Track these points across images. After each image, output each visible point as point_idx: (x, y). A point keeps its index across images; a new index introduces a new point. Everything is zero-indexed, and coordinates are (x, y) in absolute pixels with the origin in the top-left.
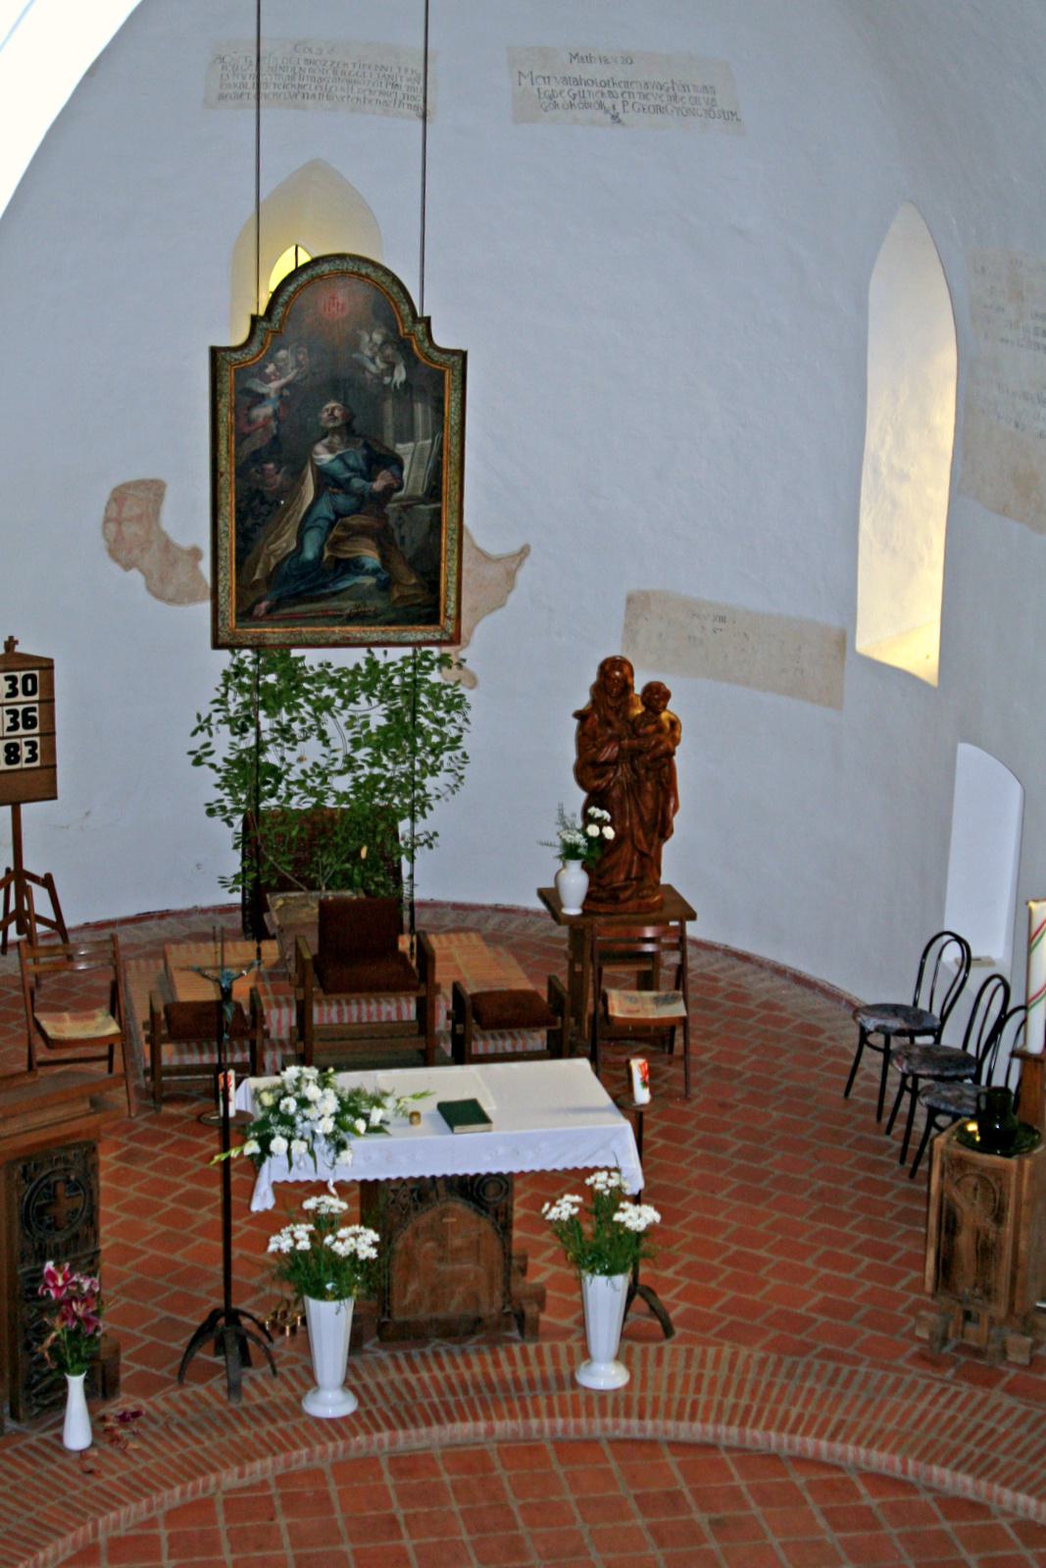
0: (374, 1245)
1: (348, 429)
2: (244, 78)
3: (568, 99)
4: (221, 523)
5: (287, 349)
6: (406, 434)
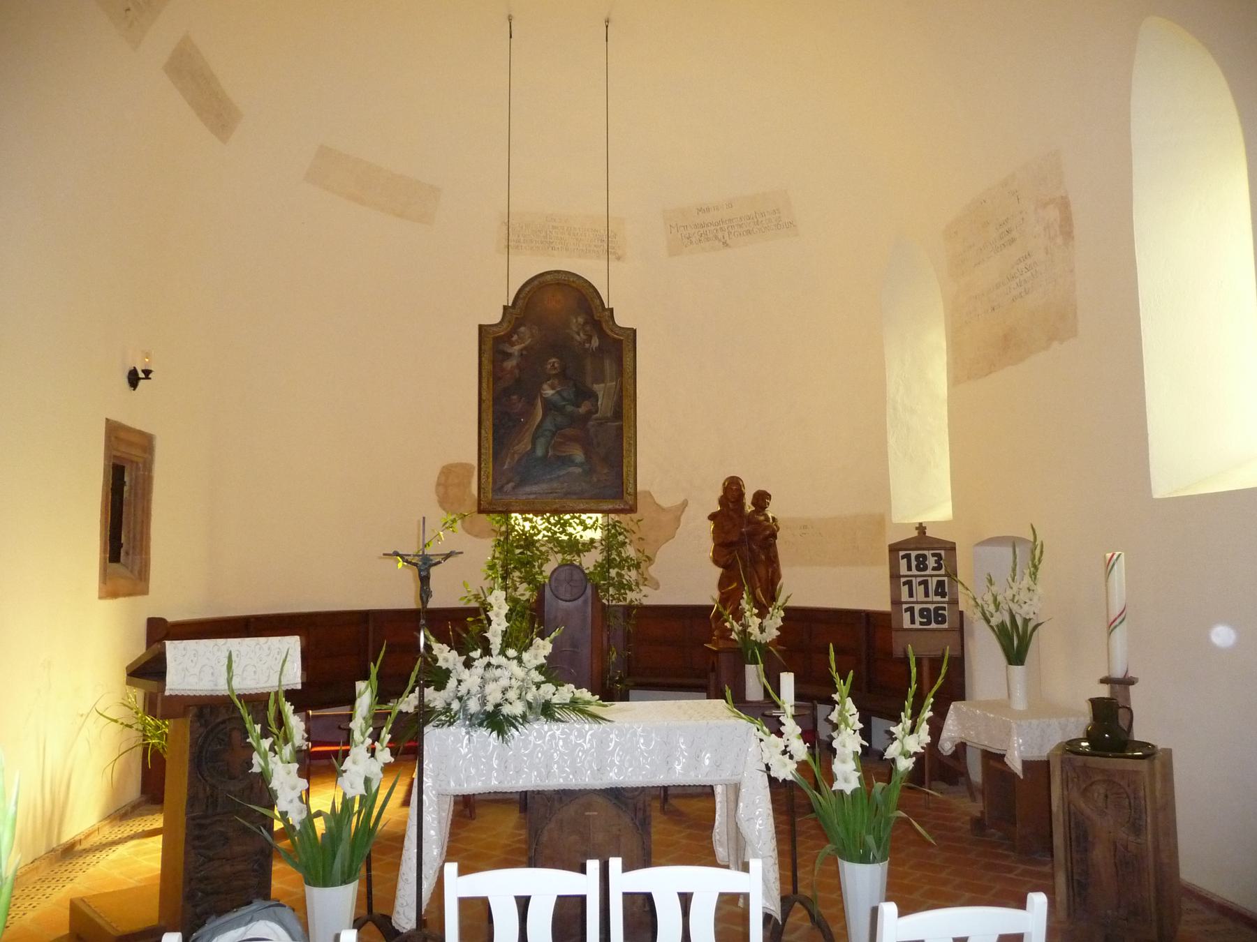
0: (291, 705)
1: (563, 375)
2: (519, 236)
3: (698, 237)
4: (483, 432)
5: (525, 326)
6: (600, 379)
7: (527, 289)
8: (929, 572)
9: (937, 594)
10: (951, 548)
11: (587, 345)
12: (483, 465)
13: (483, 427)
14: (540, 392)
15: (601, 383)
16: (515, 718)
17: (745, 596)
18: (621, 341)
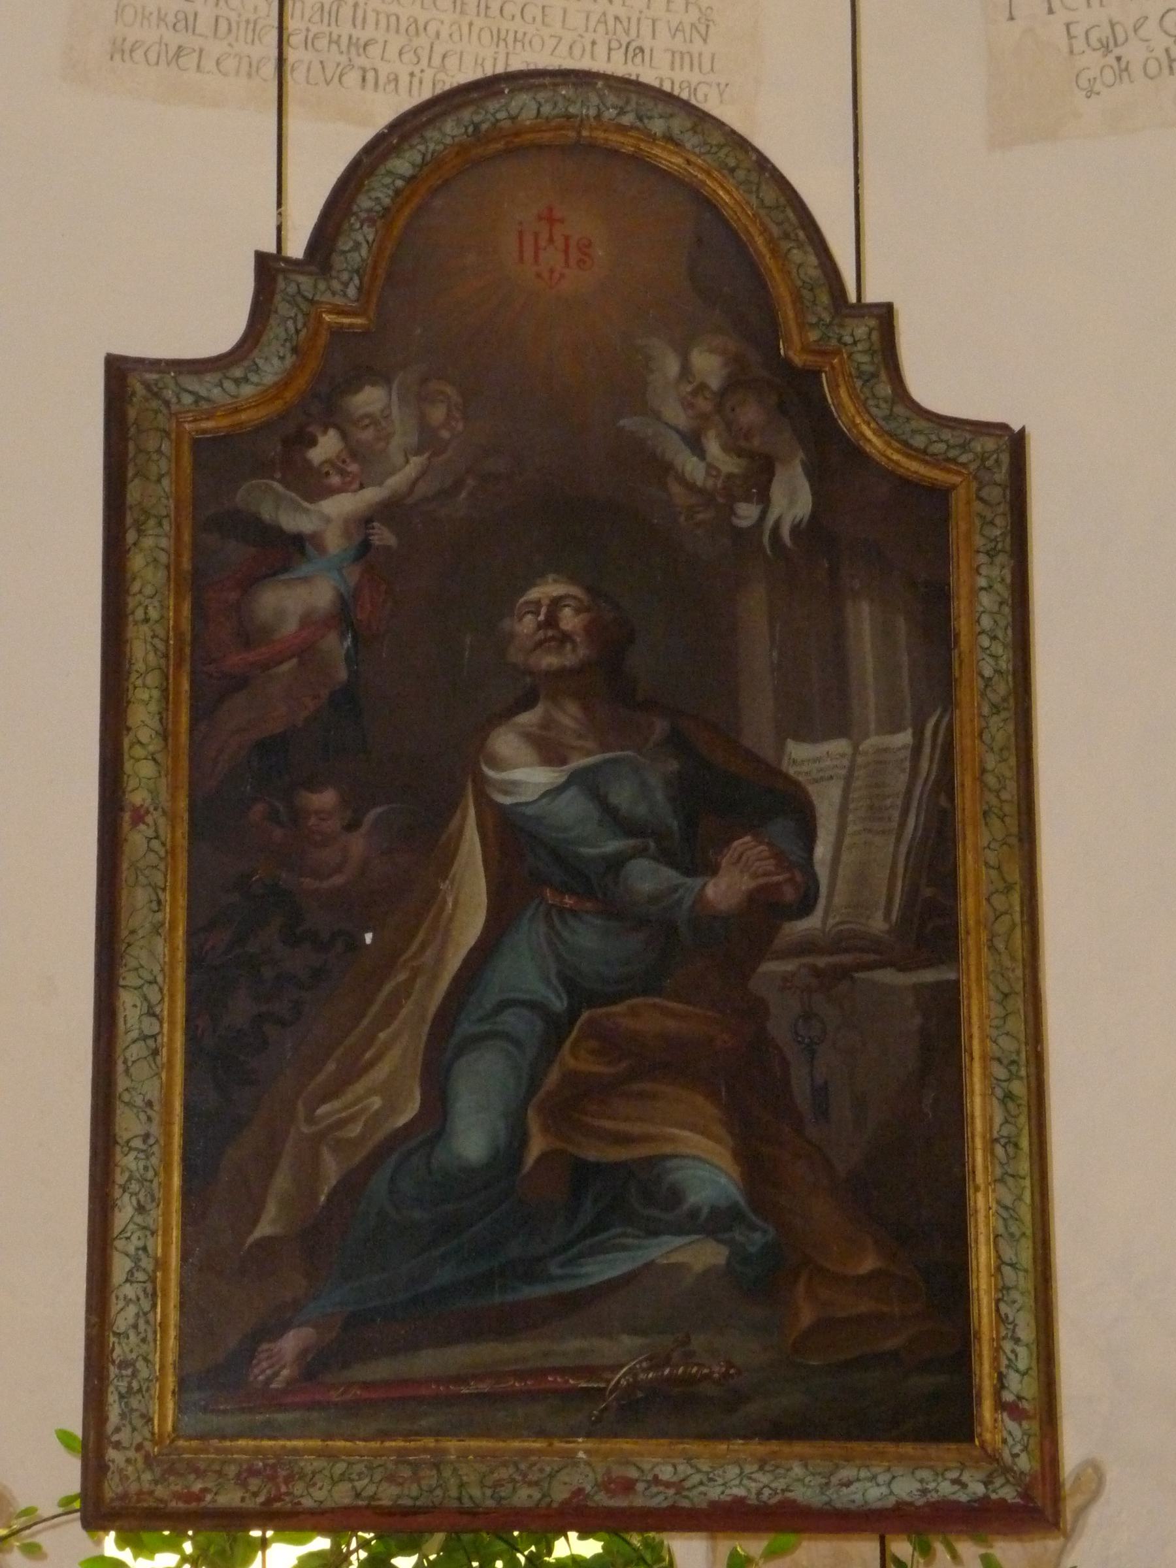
5: (383, 378)
7: (402, 165)
11: (747, 513)
12: (124, 1214)
13: (129, 979)
14: (481, 782)
15: (826, 737)
18: (940, 495)
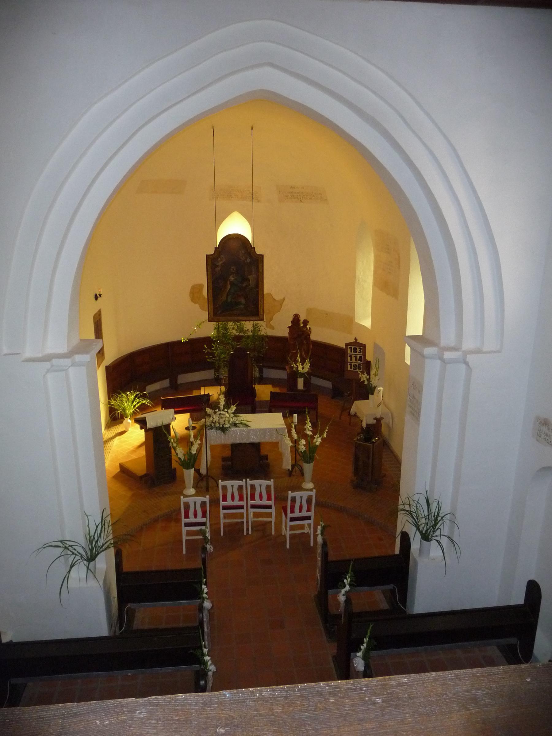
4: (209, 294)
8: (357, 353)
9: (359, 360)
10: (364, 346)
16: (227, 428)
17: (298, 356)
